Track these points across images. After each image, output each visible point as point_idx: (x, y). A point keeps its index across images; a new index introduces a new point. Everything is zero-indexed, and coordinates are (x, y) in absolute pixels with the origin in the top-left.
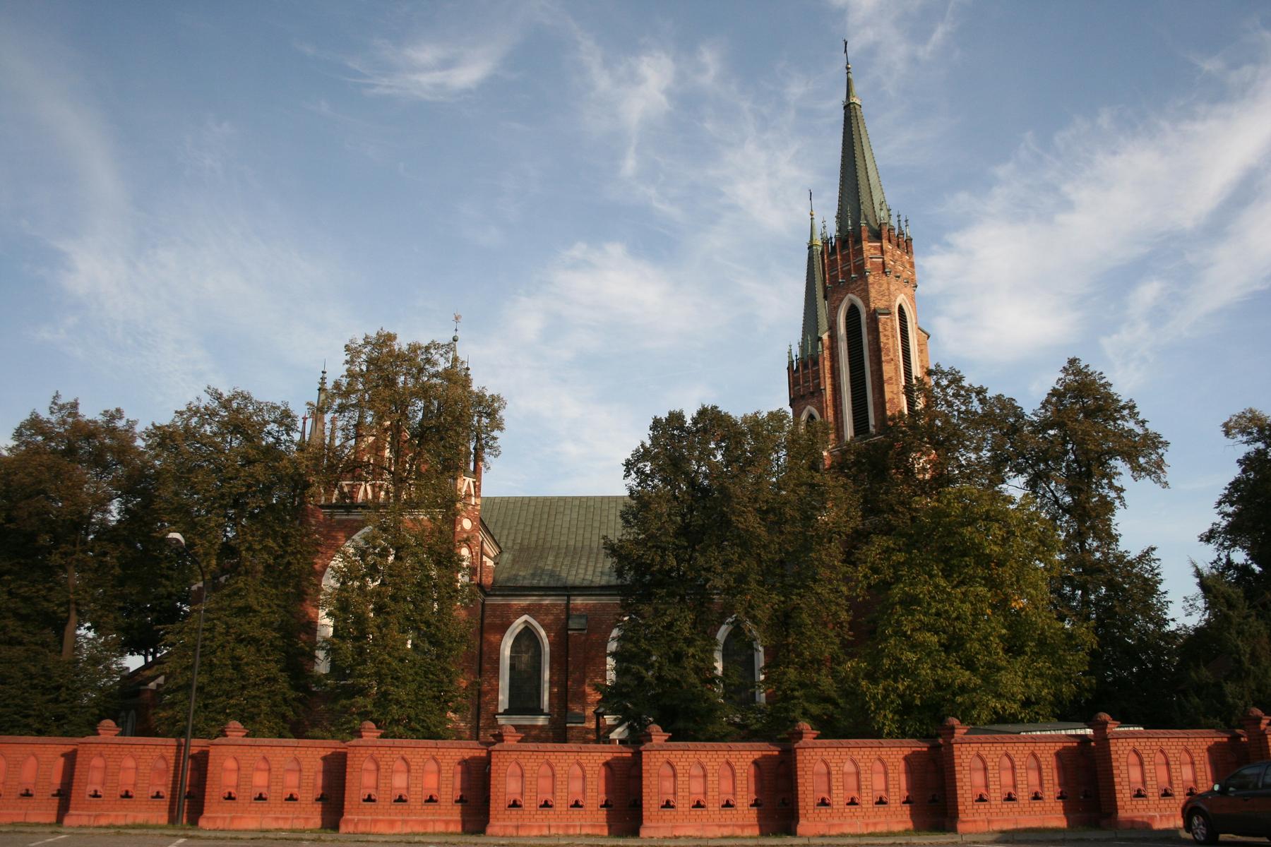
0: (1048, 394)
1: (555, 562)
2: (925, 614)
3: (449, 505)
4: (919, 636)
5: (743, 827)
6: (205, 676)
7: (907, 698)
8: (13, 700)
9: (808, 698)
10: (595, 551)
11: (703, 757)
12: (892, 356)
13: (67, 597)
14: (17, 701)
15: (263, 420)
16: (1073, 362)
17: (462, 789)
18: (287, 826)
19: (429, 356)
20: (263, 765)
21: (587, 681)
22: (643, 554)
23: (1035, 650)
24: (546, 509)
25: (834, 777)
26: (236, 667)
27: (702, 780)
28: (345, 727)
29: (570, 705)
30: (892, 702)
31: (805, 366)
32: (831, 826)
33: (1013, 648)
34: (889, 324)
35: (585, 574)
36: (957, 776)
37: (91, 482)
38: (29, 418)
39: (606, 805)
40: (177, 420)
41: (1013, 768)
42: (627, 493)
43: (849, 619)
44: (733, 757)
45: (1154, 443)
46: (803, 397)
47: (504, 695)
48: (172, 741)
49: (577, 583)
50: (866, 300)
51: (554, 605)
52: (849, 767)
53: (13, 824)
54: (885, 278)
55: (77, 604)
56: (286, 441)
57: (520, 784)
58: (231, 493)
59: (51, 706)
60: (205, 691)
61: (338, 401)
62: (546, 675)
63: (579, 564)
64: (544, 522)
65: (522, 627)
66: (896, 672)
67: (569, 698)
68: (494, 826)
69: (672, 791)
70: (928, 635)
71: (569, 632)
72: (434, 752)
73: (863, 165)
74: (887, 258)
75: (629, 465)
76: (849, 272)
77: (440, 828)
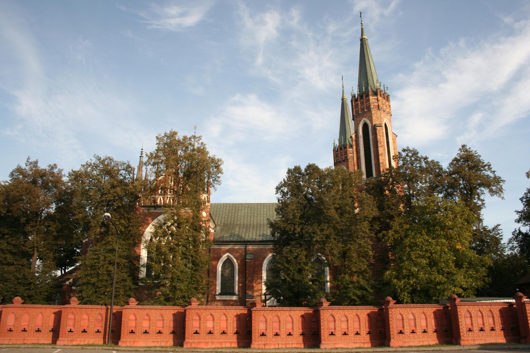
0: (453, 160)
1: (239, 231)
2: (420, 251)
3: (198, 206)
4: (419, 260)
5: (364, 343)
6: (96, 279)
7: (415, 287)
8: (11, 289)
9: (355, 288)
10: (256, 226)
11: (347, 312)
12: (382, 144)
13: (33, 245)
14: (12, 289)
15: (119, 169)
16: (463, 146)
17: (237, 328)
18: (158, 345)
19: (191, 142)
20: (147, 318)
21: (254, 281)
22: (286, 227)
23: (467, 266)
24: (234, 209)
25: (405, 321)
26: (109, 275)
27: (346, 323)
28: (157, 300)
29: (247, 291)
30: (408, 289)
31: (341, 149)
32: (405, 342)
33: (458, 265)
34: (381, 131)
35: (252, 236)
36: (459, 320)
37: (42, 195)
38: (16, 168)
39: (302, 334)
40: (82, 168)
41: (482, 316)
42: (277, 202)
43: (373, 254)
44: (359, 312)
45: (498, 180)
46: (340, 162)
47: (218, 287)
48: (104, 307)
49: (249, 239)
50: (371, 121)
51: (240, 249)
52: (411, 317)
53: (33, 344)
54: (379, 112)
55: (37, 248)
56: (128, 178)
57: (265, 325)
58: (106, 200)
59: (27, 291)
60: (96, 285)
61: (153, 160)
62: (237, 278)
63: (249, 231)
64: (233, 214)
65: (226, 258)
66: (409, 276)
67: (247, 288)
68: (254, 344)
69: (333, 328)
70: (423, 260)
71: (247, 260)
72: (224, 311)
73: (369, 64)
74: (380, 103)
75: (278, 189)
76: (363, 109)
77: (228, 345)
